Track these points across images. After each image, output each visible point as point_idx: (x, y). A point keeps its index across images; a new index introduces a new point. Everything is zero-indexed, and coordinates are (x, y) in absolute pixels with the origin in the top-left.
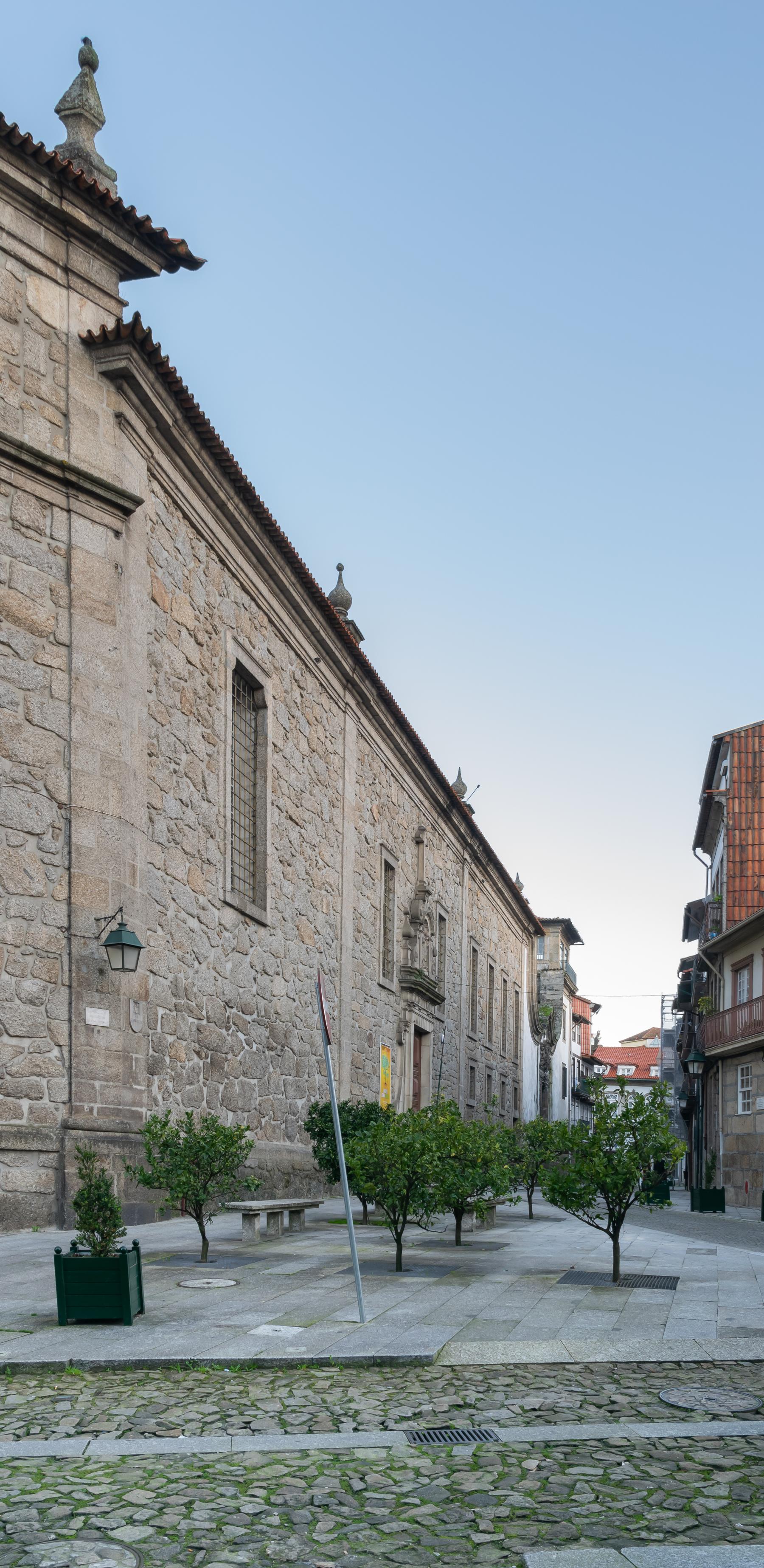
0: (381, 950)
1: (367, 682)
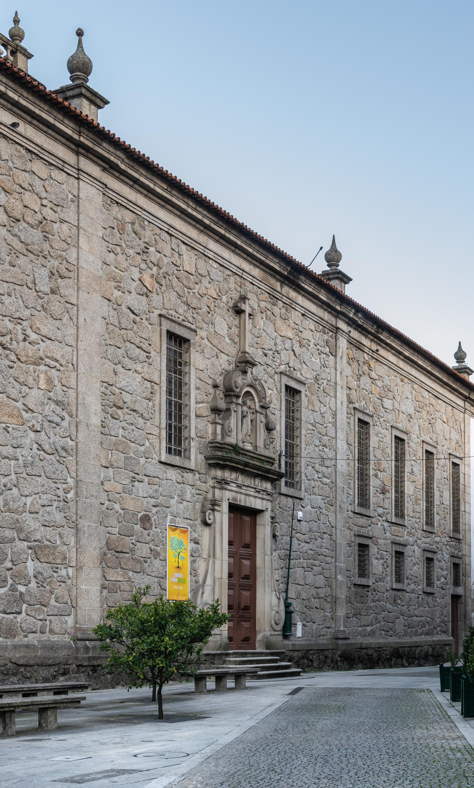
0: (164, 425)
1: (104, 145)
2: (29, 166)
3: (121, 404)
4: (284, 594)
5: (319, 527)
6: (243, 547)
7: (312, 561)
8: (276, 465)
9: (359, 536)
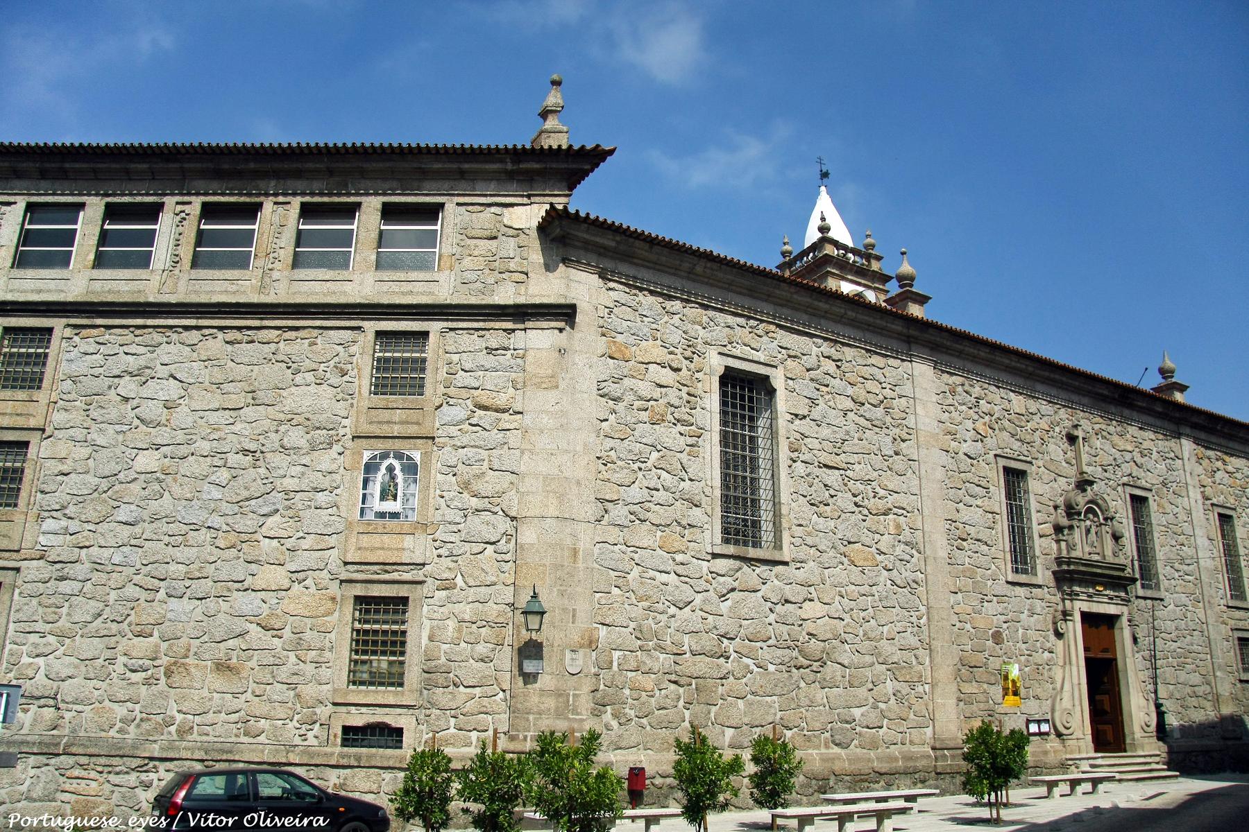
0: (1008, 549)
2: (870, 361)
3: (965, 536)
4: (1153, 695)
5: (1186, 624)
6: (1102, 652)
7: (1182, 659)
8: (1129, 570)
9: (1237, 629)
